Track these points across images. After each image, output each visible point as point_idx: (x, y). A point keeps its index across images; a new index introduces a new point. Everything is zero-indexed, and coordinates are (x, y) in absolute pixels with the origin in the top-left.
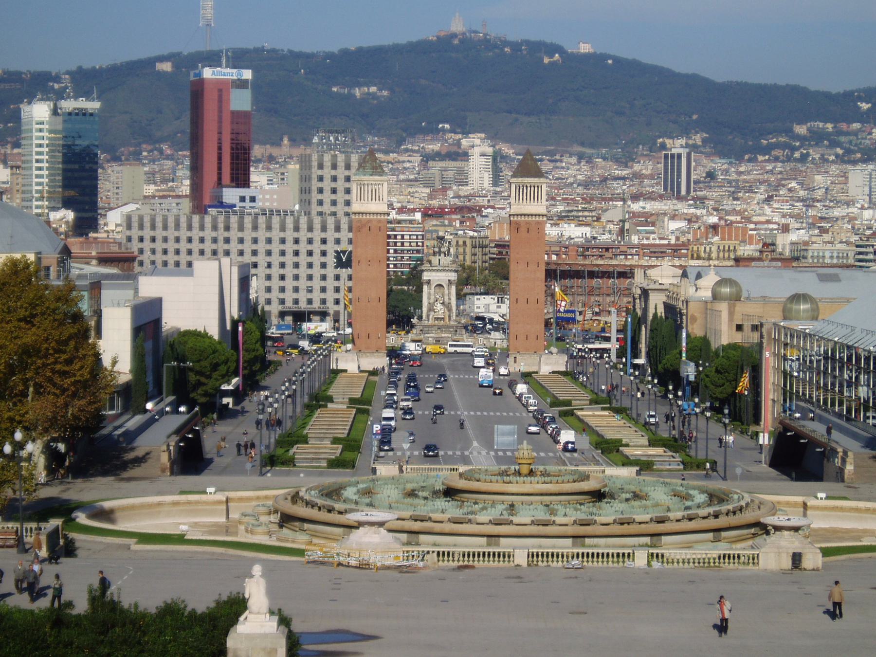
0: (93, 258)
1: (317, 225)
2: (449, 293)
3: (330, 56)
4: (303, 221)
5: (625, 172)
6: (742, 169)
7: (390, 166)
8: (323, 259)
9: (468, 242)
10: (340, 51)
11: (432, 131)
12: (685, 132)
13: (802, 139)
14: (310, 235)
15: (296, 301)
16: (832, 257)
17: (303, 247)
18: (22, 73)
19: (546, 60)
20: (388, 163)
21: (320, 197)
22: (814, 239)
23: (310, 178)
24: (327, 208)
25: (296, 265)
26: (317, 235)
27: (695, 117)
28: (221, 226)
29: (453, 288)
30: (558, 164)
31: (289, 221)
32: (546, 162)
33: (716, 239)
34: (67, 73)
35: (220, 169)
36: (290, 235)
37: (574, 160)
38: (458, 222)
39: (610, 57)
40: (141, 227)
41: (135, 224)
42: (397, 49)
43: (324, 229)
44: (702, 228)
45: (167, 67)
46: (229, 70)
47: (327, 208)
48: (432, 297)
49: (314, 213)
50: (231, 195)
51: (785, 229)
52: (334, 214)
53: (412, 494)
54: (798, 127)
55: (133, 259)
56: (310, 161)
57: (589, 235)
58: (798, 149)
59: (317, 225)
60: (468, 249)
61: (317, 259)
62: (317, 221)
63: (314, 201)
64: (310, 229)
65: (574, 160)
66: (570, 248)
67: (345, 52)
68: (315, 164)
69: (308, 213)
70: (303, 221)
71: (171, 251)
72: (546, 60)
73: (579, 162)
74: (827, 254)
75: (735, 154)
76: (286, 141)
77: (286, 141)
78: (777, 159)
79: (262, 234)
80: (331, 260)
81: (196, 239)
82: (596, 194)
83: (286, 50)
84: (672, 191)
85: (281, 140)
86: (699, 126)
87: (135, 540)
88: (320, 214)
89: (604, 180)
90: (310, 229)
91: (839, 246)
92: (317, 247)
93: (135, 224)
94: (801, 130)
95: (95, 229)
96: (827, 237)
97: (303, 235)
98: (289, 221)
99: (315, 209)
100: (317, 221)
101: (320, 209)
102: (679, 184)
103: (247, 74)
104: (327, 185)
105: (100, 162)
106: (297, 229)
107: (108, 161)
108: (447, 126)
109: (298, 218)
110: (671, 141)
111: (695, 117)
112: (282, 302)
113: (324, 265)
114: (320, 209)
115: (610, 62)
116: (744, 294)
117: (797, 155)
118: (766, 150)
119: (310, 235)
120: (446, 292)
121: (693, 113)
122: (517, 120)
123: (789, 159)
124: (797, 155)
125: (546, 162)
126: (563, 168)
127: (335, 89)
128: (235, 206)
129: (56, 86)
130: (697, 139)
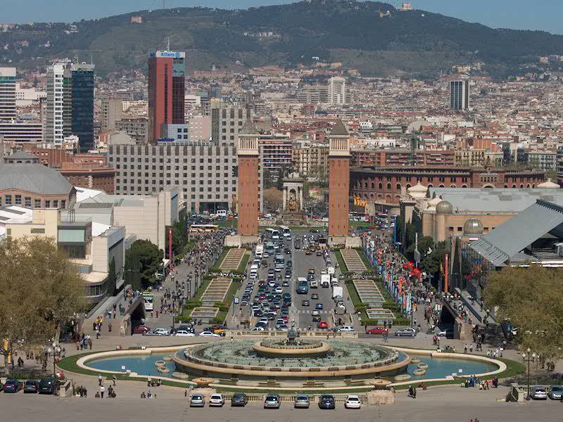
0: (90, 174)
1: (222, 152)
2: (299, 195)
3: (242, 12)
4: (214, 149)
5: (430, 90)
6: (505, 87)
7: (281, 85)
8: (185, 171)
9: (319, 150)
10: (250, 9)
11: (308, 63)
12: (471, 62)
13: (546, 66)
14: (185, 157)
15: (210, 197)
16: (543, 159)
17: (214, 172)
18: (46, 24)
19: (382, 15)
20: (280, 82)
21: (224, 134)
22: (532, 147)
23: (218, 123)
24: (228, 141)
25: (210, 182)
26: (222, 157)
27: (476, 52)
28: (165, 152)
29: (301, 191)
30: (388, 84)
31: (206, 149)
32: (380, 82)
33: (471, 147)
34: (74, 24)
35: (166, 103)
36: (206, 157)
37: (398, 81)
38: (315, 135)
39: (423, 12)
40: (118, 152)
41: (115, 151)
42: (286, 7)
43: (226, 153)
44: (464, 140)
45: (139, 20)
46: (172, 52)
47: (228, 141)
48: (289, 197)
49: (220, 144)
50: (172, 130)
51: (516, 140)
52: (232, 144)
53: (237, 353)
54: (542, 58)
55: (111, 175)
56: (218, 113)
57: (395, 144)
58: (542, 72)
59: (222, 152)
60: (319, 155)
61: (222, 172)
62: (222, 149)
63: (221, 137)
64: (218, 154)
65: (398, 81)
66: (382, 154)
67: (252, 9)
68: (221, 115)
69: (217, 144)
70: (214, 149)
71: (136, 166)
72: (382, 15)
73: (401, 82)
74: (540, 157)
75: (498, 78)
76: (214, 68)
77: (214, 68)
78: (529, 79)
79: (189, 157)
80: (230, 172)
81: (150, 160)
82: (408, 103)
83: (214, 8)
84: (456, 108)
85: (211, 67)
86: (480, 57)
87: (106, 378)
88: (224, 144)
89: (416, 96)
90: (218, 154)
91: (547, 152)
92: (222, 165)
93: (115, 151)
94: (544, 60)
95: (92, 147)
96: (541, 146)
97: (214, 157)
98: (206, 149)
99: (221, 141)
100: (222, 149)
101: (224, 141)
102: (461, 103)
103: (182, 55)
104: (228, 127)
105: (96, 82)
106: (210, 153)
107: (101, 82)
108: (317, 58)
109: (211, 148)
110: (461, 68)
111: (476, 52)
112: (202, 197)
113: (226, 175)
114: (224, 141)
115: (423, 15)
116: (455, 209)
117: (542, 77)
118: (523, 73)
119: (218, 157)
120: (297, 194)
121: (475, 49)
122: (362, 54)
123: (537, 80)
124: (542, 77)
125: (380, 82)
126: (391, 86)
127: (246, 34)
128: (173, 140)
129: (68, 32)
130: (478, 66)
